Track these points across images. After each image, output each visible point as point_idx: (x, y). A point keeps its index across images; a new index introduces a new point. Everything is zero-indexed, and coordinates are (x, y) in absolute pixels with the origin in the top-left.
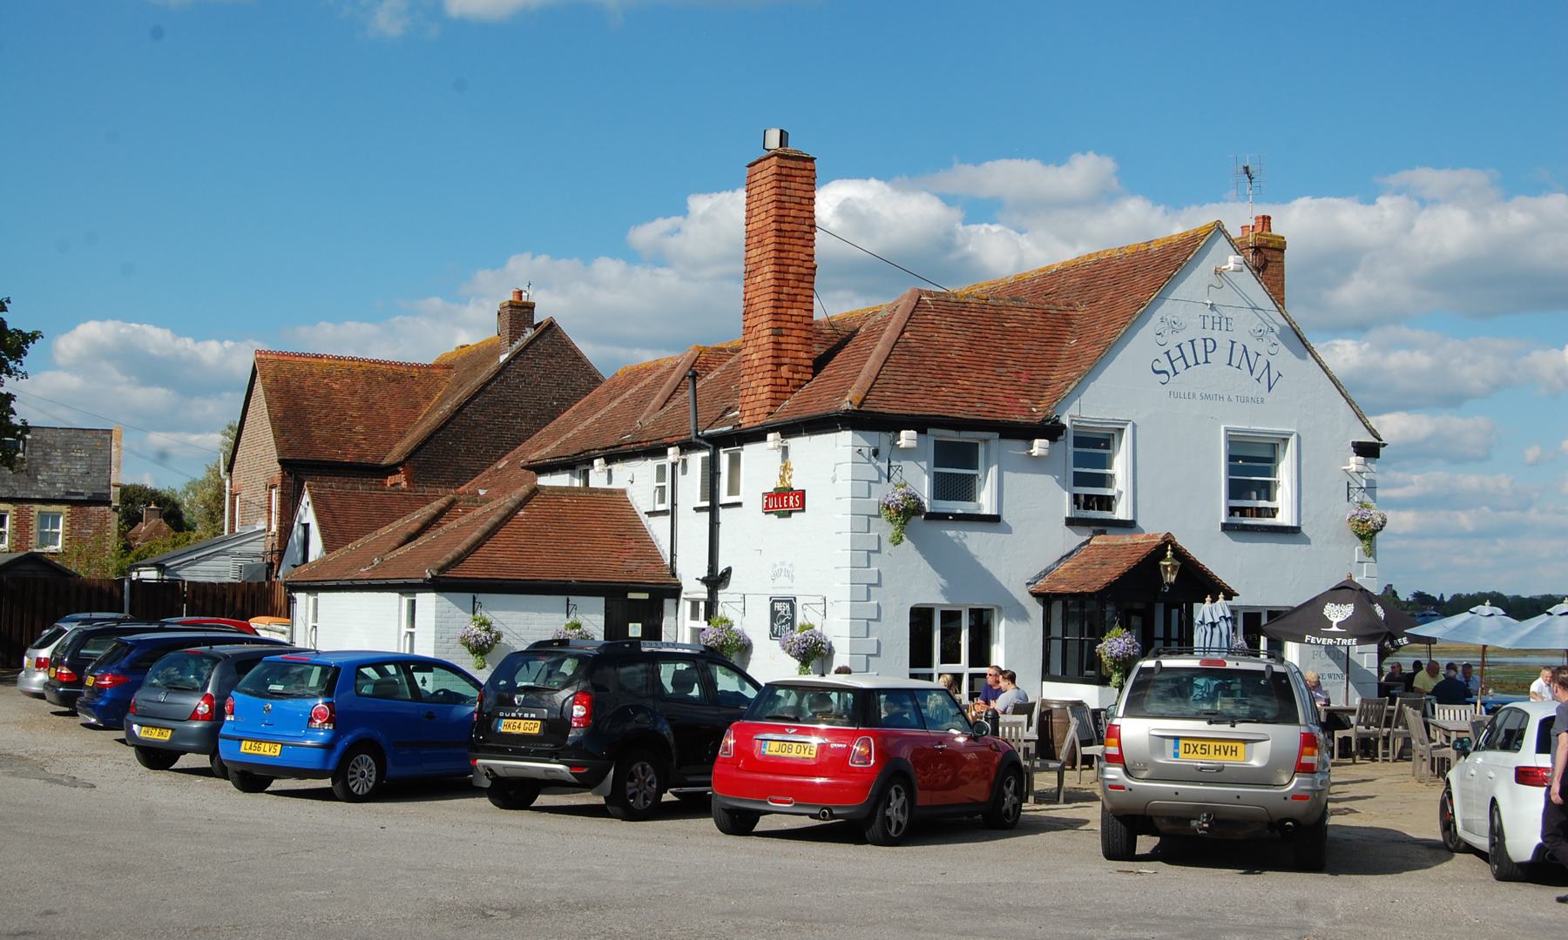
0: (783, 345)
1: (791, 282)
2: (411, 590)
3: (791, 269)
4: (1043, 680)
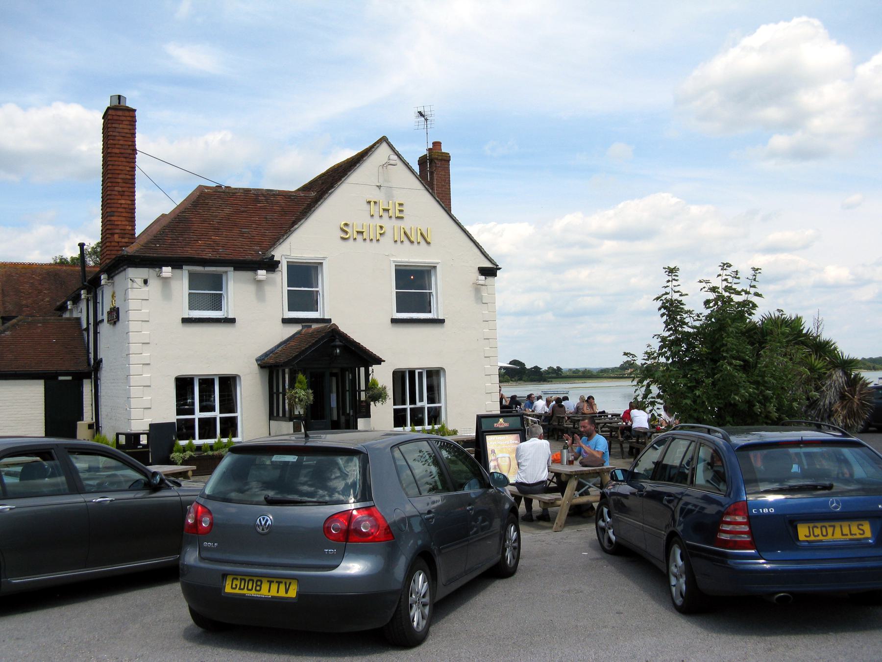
0: (116, 222)
1: (120, 184)
2: (274, 600)
3: (120, 176)
4: (270, 420)
